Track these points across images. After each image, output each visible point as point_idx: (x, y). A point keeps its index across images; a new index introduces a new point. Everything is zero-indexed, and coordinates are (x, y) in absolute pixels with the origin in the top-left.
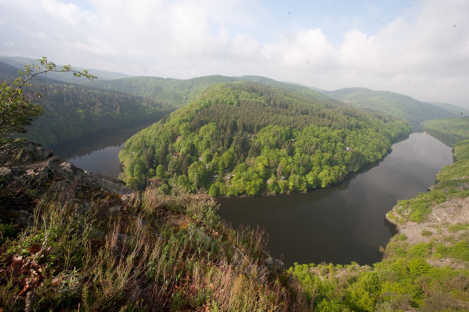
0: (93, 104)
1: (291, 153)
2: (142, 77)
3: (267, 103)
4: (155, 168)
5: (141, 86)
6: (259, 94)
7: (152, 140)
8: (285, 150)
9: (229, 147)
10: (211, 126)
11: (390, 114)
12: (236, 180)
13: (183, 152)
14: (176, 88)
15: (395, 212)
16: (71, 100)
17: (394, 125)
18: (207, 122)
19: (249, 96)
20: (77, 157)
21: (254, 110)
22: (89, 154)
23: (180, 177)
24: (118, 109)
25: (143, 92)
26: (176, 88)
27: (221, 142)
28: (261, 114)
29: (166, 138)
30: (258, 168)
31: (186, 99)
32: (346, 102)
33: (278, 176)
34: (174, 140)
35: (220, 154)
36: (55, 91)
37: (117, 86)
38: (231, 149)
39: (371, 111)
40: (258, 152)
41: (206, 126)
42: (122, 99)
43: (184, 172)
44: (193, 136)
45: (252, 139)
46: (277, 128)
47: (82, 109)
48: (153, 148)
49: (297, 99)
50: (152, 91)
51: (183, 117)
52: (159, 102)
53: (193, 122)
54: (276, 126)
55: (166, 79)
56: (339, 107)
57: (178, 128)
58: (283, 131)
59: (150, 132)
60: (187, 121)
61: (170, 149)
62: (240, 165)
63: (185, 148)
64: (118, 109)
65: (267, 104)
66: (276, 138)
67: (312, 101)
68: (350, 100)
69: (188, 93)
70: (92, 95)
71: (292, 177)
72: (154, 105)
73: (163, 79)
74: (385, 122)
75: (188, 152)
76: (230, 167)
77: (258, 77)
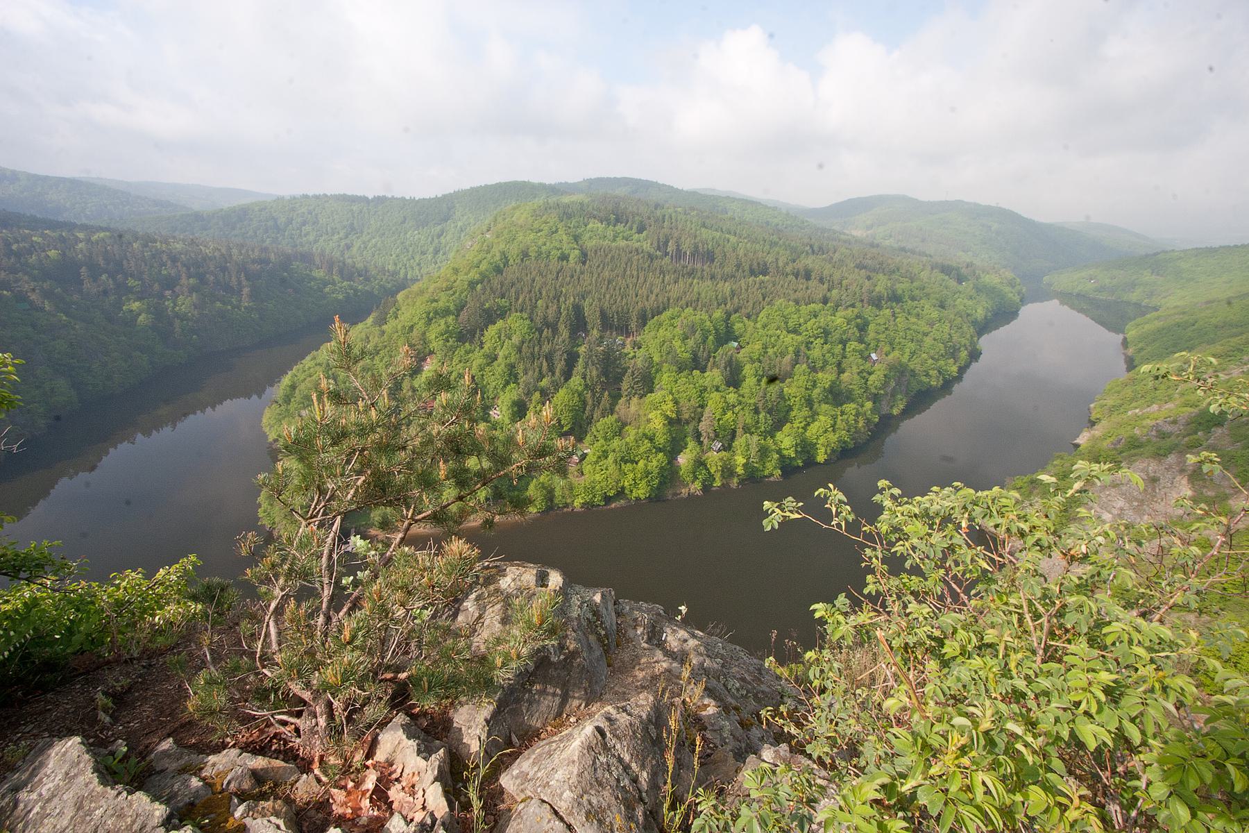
0: (170, 283)
1: (734, 379)
2: (306, 197)
3: (659, 248)
5: (304, 223)
6: (635, 227)
9: (568, 375)
12: (597, 462)
14: (403, 222)
16: (104, 277)
19: (610, 233)
21: (625, 271)
24: (246, 291)
26: (403, 222)
27: (545, 364)
30: (651, 426)
31: (436, 252)
32: (858, 233)
33: (706, 441)
36: (53, 253)
38: (576, 381)
42: (254, 262)
44: (467, 352)
47: (139, 299)
50: (336, 237)
51: (434, 304)
52: (360, 265)
53: (464, 315)
54: (689, 310)
57: (424, 334)
58: (708, 323)
60: (446, 312)
64: (246, 291)
66: (691, 342)
68: (869, 228)
70: (165, 258)
72: (348, 273)
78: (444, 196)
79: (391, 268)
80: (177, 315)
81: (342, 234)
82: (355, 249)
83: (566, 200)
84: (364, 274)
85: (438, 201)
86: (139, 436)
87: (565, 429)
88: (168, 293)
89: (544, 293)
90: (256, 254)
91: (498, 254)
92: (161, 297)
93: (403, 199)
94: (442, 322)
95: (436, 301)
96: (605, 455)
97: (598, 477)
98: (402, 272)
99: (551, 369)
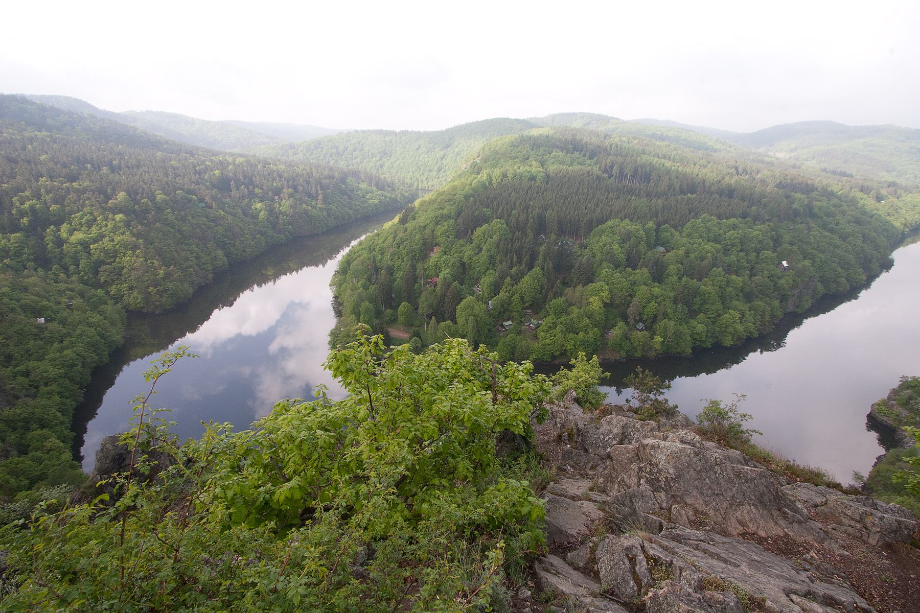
0: (278, 192)
1: (659, 275)
2: (356, 132)
3: (605, 171)
4: (395, 308)
5: (355, 150)
6: (588, 154)
7: (387, 257)
8: (645, 270)
9: (530, 267)
10: (498, 225)
11: (891, 180)
12: (547, 331)
13: (445, 279)
14: (418, 149)
15: (894, 402)
16: (243, 187)
17: (900, 204)
18: (486, 220)
19: (568, 160)
20: (255, 286)
21: (578, 189)
22: (275, 281)
23: (442, 324)
24: (320, 197)
25: (359, 161)
26: (418, 149)
27: (515, 257)
28: (593, 197)
29: (411, 251)
30: (590, 307)
31: (439, 170)
32: (781, 155)
33: (632, 322)
34: (425, 256)
35: (516, 280)
36: (217, 172)
37: (312, 154)
38: (537, 270)
39: (844, 174)
40: (589, 278)
41: (485, 227)
42: (325, 178)
43: (447, 316)
44: (462, 246)
45: (576, 248)
46: (627, 225)
47: (261, 201)
48: (390, 271)
49: (669, 159)
50: (374, 159)
51: (441, 211)
52: (389, 180)
53: (460, 220)
54: (627, 221)
55: (400, 133)
56: (766, 172)
57: (433, 231)
58: (642, 232)
59: (381, 241)
60: (448, 217)
61: (419, 272)
62: (554, 301)
63: (448, 270)
64: (320, 197)
65: (605, 175)
66: (626, 246)
67: (703, 162)
68: (792, 151)
69: (442, 159)
70: (275, 175)
71: (661, 324)
72: (380, 185)
73: (394, 133)
74: (879, 199)
75: (455, 277)
76: (536, 306)
77: (583, 115)
78: (447, 130)
79: (408, 181)
80: (281, 213)
81: (378, 158)
82: (385, 168)
83: (535, 132)
84: (392, 186)
85: (442, 133)
86: (255, 286)
87: (527, 305)
88: (276, 198)
89: (517, 204)
90: (326, 173)
91: (485, 175)
92: (273, 200)
93: (419, 132)
94: (446, 223)
95: (442, 209)
96: (554, 325)
97: (548, 341)
98: (416, 184)
99: (520, 261)
